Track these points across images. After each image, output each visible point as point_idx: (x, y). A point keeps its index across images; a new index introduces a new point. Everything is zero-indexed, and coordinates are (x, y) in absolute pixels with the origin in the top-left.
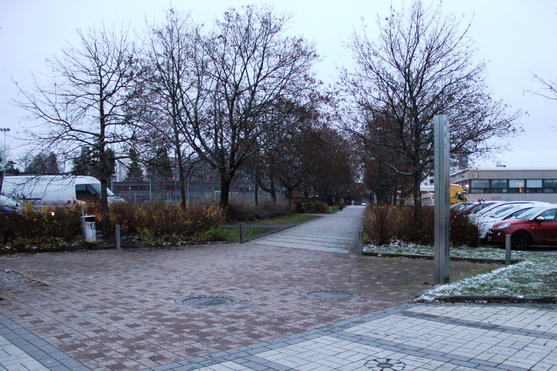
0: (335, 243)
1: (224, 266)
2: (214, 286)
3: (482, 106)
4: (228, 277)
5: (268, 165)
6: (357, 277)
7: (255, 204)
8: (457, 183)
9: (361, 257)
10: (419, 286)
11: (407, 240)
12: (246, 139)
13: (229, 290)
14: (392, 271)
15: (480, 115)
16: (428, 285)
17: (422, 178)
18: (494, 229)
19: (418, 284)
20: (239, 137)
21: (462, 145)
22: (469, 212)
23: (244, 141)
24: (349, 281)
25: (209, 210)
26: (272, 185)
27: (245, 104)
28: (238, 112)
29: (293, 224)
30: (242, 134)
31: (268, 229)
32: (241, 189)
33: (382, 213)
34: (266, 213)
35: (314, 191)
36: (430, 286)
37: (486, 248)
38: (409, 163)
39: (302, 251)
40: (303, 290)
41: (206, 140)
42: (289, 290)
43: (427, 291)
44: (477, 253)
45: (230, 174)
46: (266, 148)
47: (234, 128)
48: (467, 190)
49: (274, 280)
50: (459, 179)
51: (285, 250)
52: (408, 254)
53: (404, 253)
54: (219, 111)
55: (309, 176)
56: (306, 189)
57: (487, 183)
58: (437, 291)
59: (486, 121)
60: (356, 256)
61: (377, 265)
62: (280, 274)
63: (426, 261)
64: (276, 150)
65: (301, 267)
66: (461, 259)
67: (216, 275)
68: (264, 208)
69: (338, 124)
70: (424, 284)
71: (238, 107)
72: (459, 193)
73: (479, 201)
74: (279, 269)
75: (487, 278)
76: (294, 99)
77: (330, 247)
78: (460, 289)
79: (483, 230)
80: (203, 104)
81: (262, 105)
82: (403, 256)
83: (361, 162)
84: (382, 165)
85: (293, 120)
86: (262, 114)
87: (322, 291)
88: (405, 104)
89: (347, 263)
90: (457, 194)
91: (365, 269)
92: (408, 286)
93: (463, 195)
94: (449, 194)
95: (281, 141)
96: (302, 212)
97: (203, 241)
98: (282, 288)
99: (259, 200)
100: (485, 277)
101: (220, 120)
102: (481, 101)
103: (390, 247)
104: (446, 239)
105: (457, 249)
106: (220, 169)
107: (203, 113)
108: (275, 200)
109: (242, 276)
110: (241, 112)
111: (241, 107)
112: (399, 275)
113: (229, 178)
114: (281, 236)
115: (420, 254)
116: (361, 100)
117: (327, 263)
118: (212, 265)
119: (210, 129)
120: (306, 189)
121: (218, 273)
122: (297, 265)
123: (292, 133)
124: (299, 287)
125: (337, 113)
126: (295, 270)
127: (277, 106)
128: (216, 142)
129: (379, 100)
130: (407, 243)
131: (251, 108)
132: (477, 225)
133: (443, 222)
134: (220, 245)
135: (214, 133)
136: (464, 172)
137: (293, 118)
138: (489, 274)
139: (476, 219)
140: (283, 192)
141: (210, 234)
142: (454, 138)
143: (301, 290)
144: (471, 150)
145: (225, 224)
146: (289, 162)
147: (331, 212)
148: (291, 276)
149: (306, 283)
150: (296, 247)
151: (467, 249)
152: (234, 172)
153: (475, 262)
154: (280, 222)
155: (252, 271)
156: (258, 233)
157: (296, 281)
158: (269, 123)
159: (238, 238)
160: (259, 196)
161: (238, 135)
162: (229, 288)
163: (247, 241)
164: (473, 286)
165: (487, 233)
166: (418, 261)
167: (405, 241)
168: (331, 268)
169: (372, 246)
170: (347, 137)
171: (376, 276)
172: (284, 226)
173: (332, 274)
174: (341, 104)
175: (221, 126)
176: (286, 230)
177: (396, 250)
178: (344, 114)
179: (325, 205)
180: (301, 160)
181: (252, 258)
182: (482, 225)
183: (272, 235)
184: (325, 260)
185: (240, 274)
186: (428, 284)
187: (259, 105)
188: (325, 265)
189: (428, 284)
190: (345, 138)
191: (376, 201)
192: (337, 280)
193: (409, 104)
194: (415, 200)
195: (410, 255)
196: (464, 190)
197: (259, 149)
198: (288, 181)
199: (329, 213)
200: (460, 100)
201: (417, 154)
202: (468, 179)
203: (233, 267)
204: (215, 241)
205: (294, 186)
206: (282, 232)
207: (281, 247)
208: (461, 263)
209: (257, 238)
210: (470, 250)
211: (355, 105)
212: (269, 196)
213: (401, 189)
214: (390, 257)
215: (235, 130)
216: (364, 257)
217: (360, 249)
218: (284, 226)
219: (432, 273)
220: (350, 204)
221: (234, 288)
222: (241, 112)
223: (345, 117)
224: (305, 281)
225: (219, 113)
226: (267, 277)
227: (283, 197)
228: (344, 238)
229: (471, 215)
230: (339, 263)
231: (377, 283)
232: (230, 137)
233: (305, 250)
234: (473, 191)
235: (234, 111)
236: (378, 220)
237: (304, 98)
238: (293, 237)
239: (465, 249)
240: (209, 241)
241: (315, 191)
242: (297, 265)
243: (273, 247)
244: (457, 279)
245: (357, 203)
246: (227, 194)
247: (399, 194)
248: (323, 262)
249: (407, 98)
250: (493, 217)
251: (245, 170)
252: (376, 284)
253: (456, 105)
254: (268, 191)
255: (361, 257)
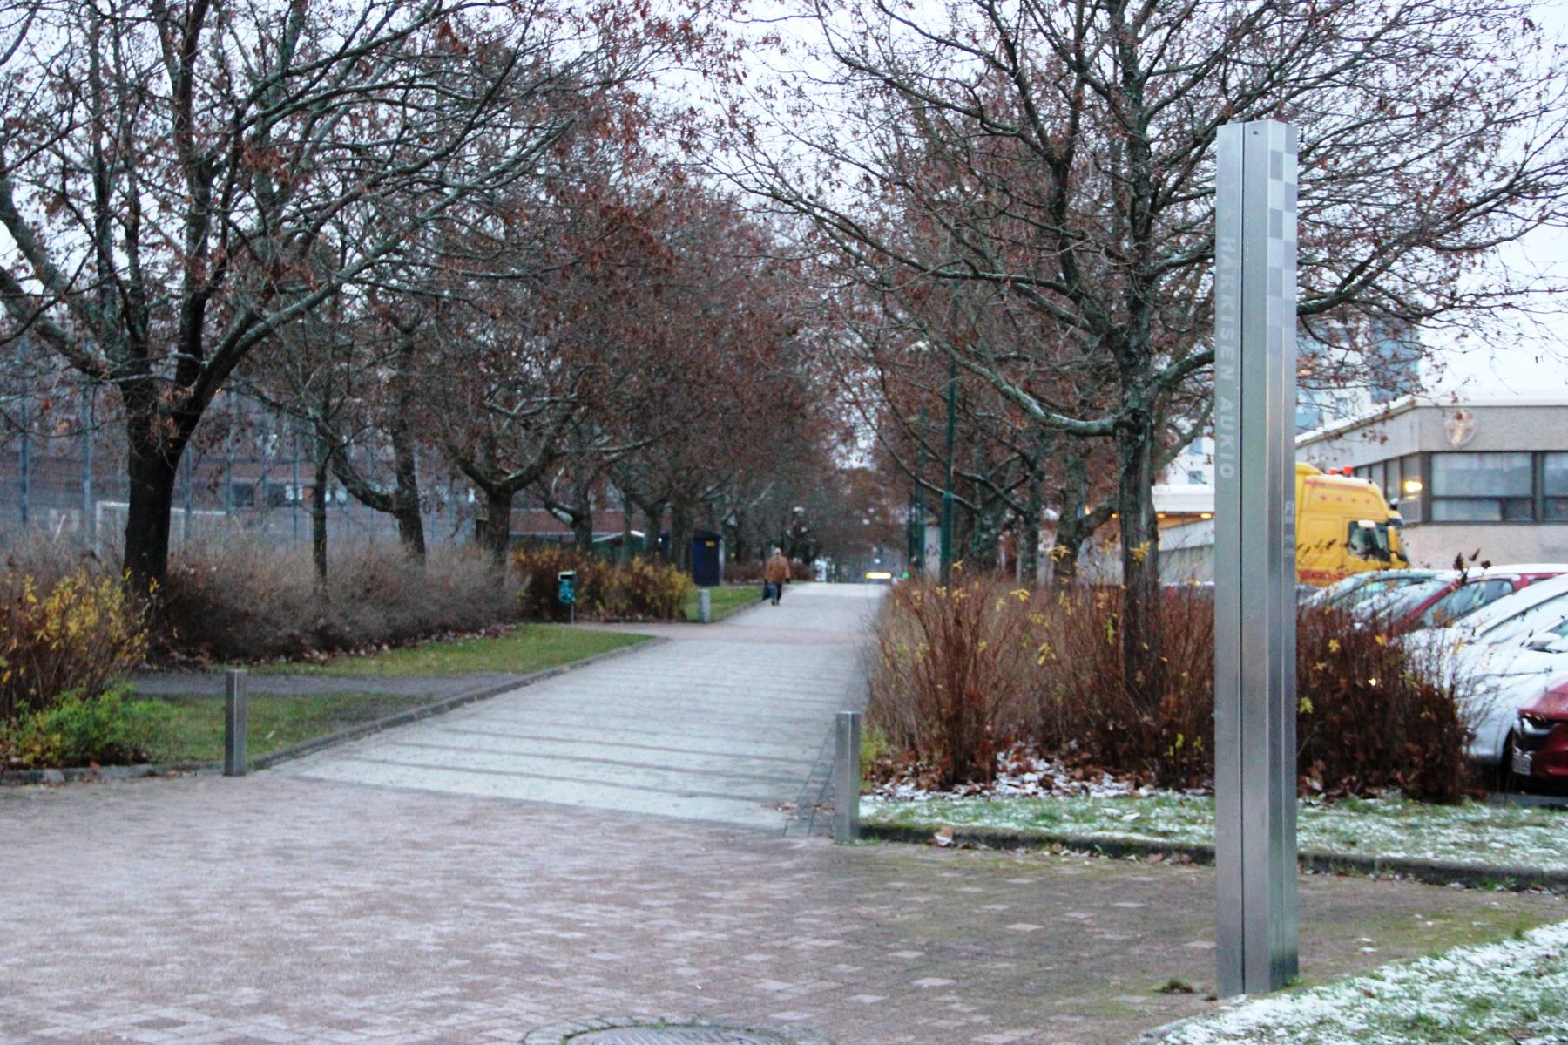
0: (718, 773)
1: (130, 896)
2: (59, 1009)
3: (1487, 66)
4: (144, 955)
5: (384, 374)
6: (820, 951)
7: (308, 571)
8: (1355, 471)
9: (850, 849)
10: (1138, 999)
11: (1087, 762)
12: (263, 234)
13: (147, 1025)
14: (1002, 918)
15: (1475, 115)
16: (1184, 997)
17: (1166, 445)
18: (1547, 709)
19: (1133, 993)
20: (228, 223)
21: (1372, 276)
22: (1412, 620)
23: (257, 244)
24: (780, 972)
25: (54, 604)
26: (405, 472)
27: (260, 51)
28: (223, 83)
29: (511, 678)
30: (247, 210)
31: (377, 700)
32: (245, 494)
33: (958, 622)
34: (372, 618)
35: (622, 510)
36: (1197, 1002)
37: (1503, 812)
38: (1099, 374)
39: (549, 818)
40: (541, 1020)
41: (46, 230)
42: (467, 1017)
43: (1179, 1028)
44: (1454, 834)
45: (178, 417)
46: (375, 286)
47: (200, 171)
48: (1409, 504)
49: (389, 968)
50: (1365, 451)
51: (463, 811)
52: (1088, 831)
53: (1069, 828)
54: (119, 78)
55: (598, 430)
56: (582, 495)
57: (1521, 469)
58: (1231, 1028)
59: (1510, 152)
60: (824, 843)
61: (926, 891)
62: (425, 936)
63: (1184, 870)
64: (426, 295)
65: (541, 895)
66: (1366, 866)
67: (78, 945)
68: (359, 592)
69: (736, 165)
70: (1164, 991)
71: (222, 61)
72: (1364, 524)
73: (1459, 564)
74: (423, 911)
75: (1503, 966)
76: (518, 30)
77: (691, 795)
78: (1353, 1024)
79: (1484, 714)
80: (23, 33)
81: (352, 57)
82: (1065, 842)
83: (859, 361)
84: (964, 378)
85: (512, 138)
86: (352, 103)
87: (637, 1024)
88: (1081, 66)
89: (770, 877)
90: (1354, 525)
91: (864, 910)
92: (1082, 1001)
93: (1384, 531)
94: (1291, 529)
95: (450, 249)
96: (561, 613)
97: (19, 766)
98: (430, 1012)
99: (333, 552)
100: (1493, 963)
101: (127, 127)
102: (1484, 41)
103: (996, 799)
104: (1275, 765)
105: (1344, 811)
106: (124, 386)
107: (23, 86)
108: (420, 547)
109: (221, 951)
110: (241, 89)
111: (237, 63)
112: (1035, 944)
113: (174, 434)
114: (446, 739)
115: (1150, 831)
116: (857, 42)
117: (673, 875)
118: (62, 895)
119: (67, 171)
120: (582, 495)
121: (89, 937)
122: (517, 890)
123: (507, 214)
124: (518, 1003)
125: (734, 109)
126: (503, 913)
127: (431, 65)
128: (101, 242)
129: (951, 42)
130: (1086, 778)
131: (290, 74)
132: (1453, 687)
133: (1262, 671)
134: (116, 784)
135: (93, 198)
136: (1388, 416)
137: (515, 135)
138: (1512, 945)
139: (1447, 655)
140: (462, 513)
141: (59, 726)
142: (1336, 239)
143: (531, 1018)
144: (1428, 302)
145: (143, 673)
146: (496, 355)
147: (707, 616)
148: (480, 943)
149: (557, 983)
150: (517, 794)
151: (1397, 814)
152: (199, 402)
153: (1441, 882)
154: (444, 667)
155: (276, 920)
156: (322, 721)
157: (504, 970)
158: (384, 151)
159: (218, 750)
160: (331, 529)
161: (225, 215)
162: (143, 1018)
163: (261, 765)
164: (1426, 1009)
165: (1512, 733)
166: (1138, 871)
167: (1075, 766)
168: (692, 902)
169: (904, 790)
170: (789, 233)
171: (922, 948)
172: (459, 686)
173: (695, 933)
174: (758, 66)
175: (132, 161)
176: (471, 708)
177: (1025, 813)
178: (769, 118)
179: (680, 579)
180: (553, 350)
181: (284, 854)
182: (1481, 688)
183: (396, 733)
184: (666, 862)
185: (210, 939)
186: (1188, 991)
187: (337, 57)
188: (666, 890)
189: (1188, 991)
190: (781, 241)
191: (933, 563)
192: (717, 968)
193: (1106, 66)
194: (1129, 562)
195: (1098, 841)
196: (1394, 507)
197: (335, 291)
198: (491, 458)
199: (699, 621)
200: (1369, 42)
201: (1137, 324)
202: (1416, 449)
203: (173, 900)
204: (85, 763)
205: (520, 483)
206: (456, 719)
207: (437, 794)
208: (1366, 886)
209: (316, 747)
210: (1413, 820)
211: (828, 67)
212: (387, 528)
213: (1061, 499)
214: (997, 848)
215: (207, 183)
216: (862, 847)
217: (843, 808)
218: (459, 686)
219: (1206, 937)
220: (804, 575)
221: (169, 1013)
222: (236, 88)
223: (776, 130)
224: (553, 973)
225: (122, 88)
226: (357, 950)
227: (460, 539)
228: (764, 750)
229: (1420, 637)
230: (731, 876)
231: (926, 982)
232: (180, 222)
233: (564, 810)
234: (1440, 510)
235: (201, 86)
236: (933, 654)
237: (568, 29)
238: (504, 744)
239: (1386, 814)
240: (51, 765)
241: (629, 510)
242: (517, 890)
243: (395, 797)
244: (1339, 970)
245: (845, 569)
246: (164, 520)
247: (1049, 524)
248: (651, 871)
249: (1090, 35)
250: (1542, 649)
251: (263, 399)
252: (919, 988)
253: (1346, 66)
254: (382, 503)
255: (850, 849)
